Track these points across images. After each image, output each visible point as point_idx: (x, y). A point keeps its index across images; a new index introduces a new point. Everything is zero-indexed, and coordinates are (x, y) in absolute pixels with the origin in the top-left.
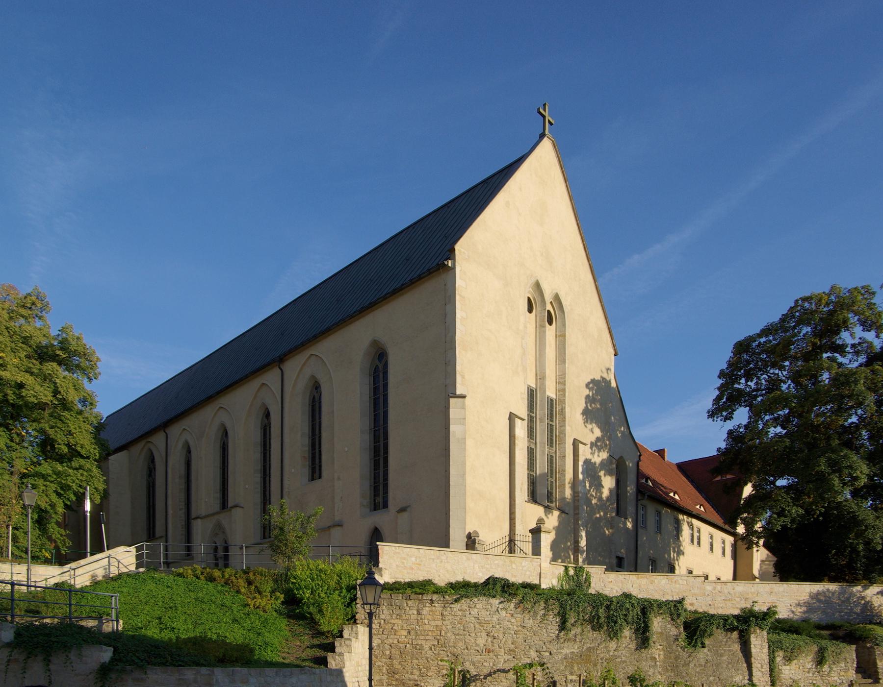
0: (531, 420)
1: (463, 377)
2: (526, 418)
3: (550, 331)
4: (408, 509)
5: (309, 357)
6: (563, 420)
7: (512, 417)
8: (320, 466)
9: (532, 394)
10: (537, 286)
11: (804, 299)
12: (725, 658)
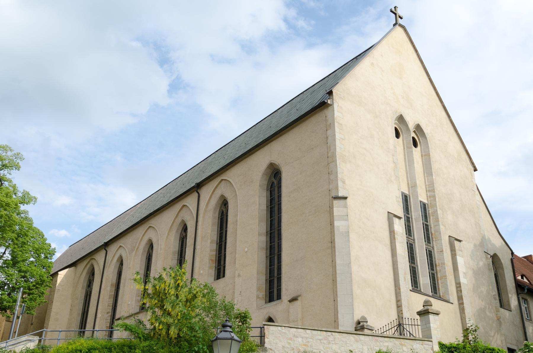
0: (408, 221)
1: (344, 183)
2: (403, 217)
3: (417, 152)
4: (299, 298)
5: (220, 182)
6: (437, 220)
7: (391, 216)
8: (224, 267)
9: (406, 199)
10: (401, 119)
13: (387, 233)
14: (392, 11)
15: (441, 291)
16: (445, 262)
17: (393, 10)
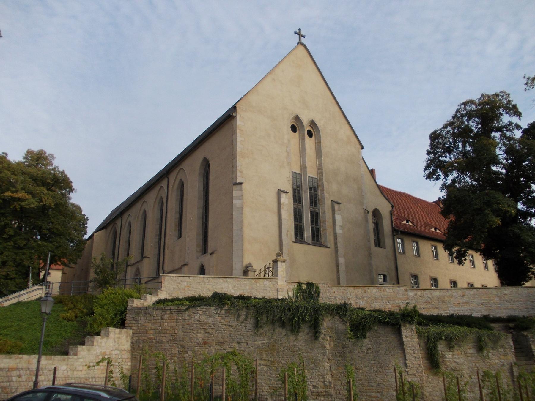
1: (242, 173)
6: (323, 190)
11: (465, 104)
12: (383, 346)
13: (275, 205)
14: (296, 33)
15: (323, 240)
16: (327, 219)
17: (298, 31)
